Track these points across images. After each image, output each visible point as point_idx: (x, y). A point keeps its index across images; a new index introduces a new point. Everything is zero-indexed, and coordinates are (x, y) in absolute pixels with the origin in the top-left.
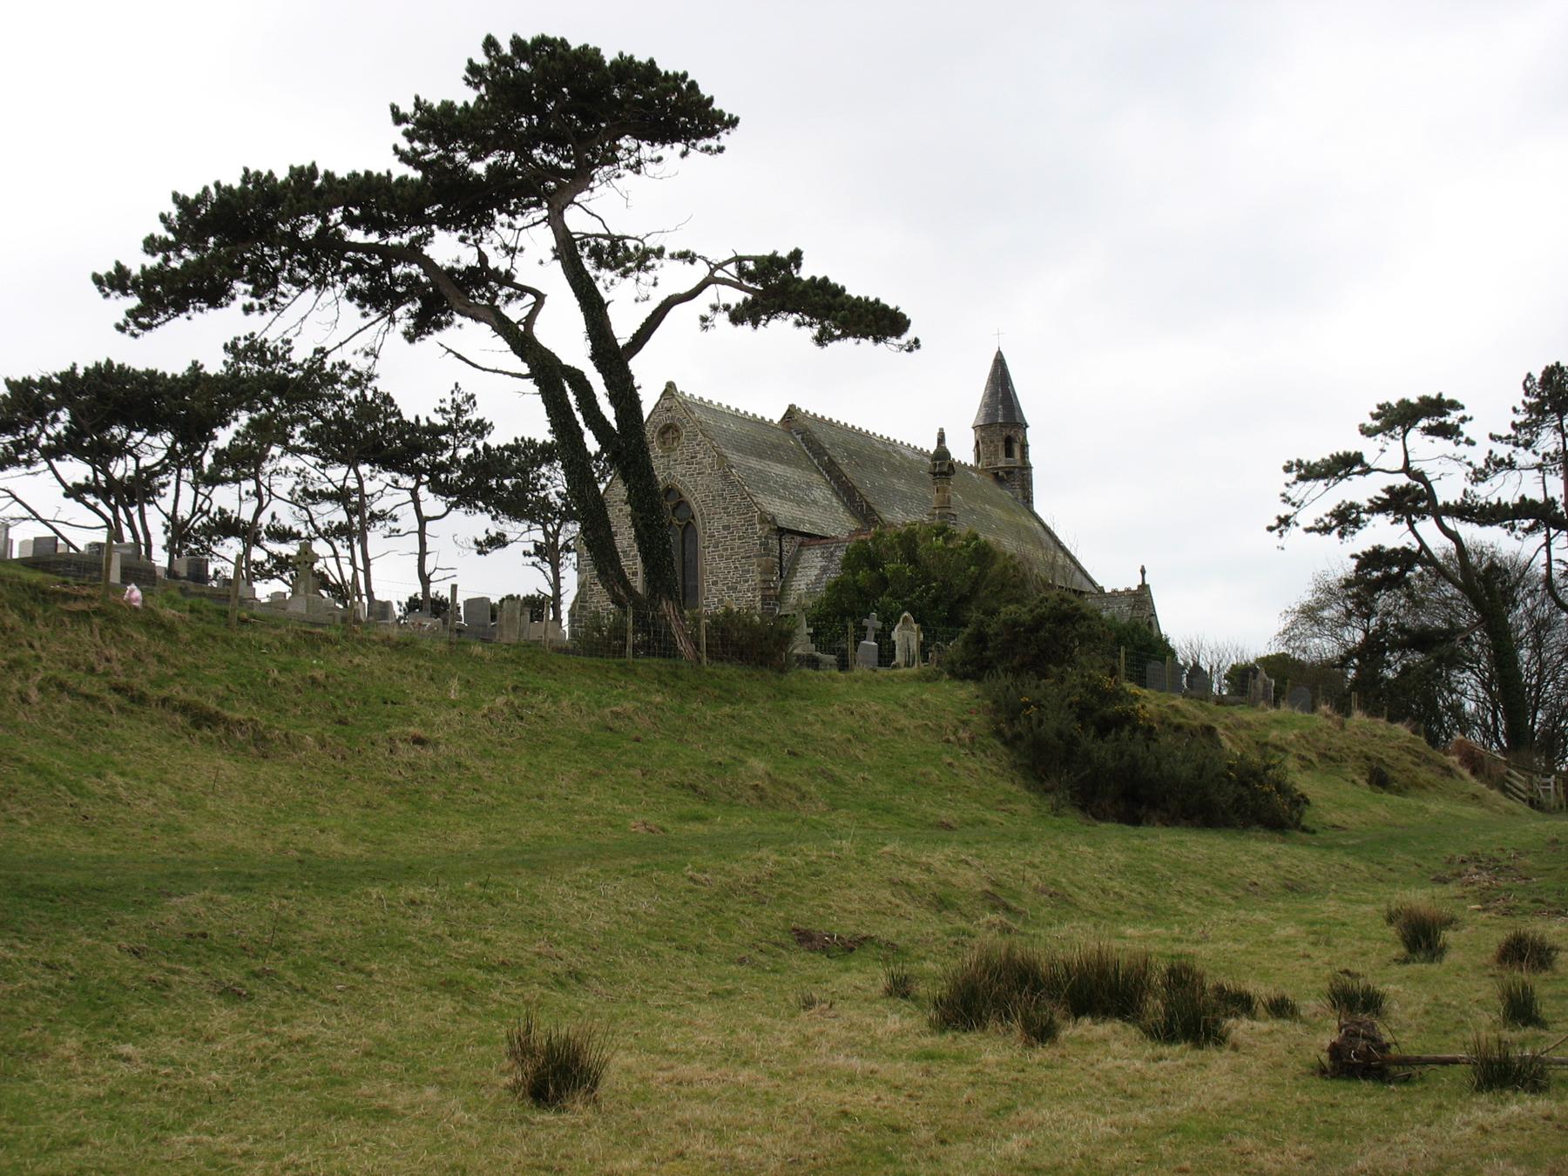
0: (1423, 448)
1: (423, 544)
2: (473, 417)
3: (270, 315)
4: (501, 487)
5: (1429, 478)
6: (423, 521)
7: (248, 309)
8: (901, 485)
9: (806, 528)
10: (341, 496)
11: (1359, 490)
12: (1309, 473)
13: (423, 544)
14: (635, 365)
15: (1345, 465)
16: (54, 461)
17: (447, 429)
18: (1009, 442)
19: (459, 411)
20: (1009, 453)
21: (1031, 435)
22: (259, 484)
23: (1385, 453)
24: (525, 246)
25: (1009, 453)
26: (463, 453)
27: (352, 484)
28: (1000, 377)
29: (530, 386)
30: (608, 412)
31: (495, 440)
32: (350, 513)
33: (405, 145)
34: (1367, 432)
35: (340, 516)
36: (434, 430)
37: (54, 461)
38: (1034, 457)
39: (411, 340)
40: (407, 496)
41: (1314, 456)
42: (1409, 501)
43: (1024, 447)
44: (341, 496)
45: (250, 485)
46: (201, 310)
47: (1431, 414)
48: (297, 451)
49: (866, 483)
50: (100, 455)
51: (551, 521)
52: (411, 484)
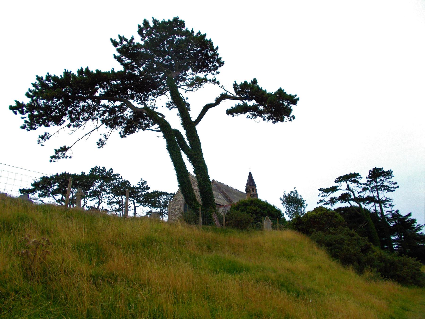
0: (352, 185)
1: (135, 212)
2: (145, 185)
3: (75, 128)
4: (151, 201)
5: (353, 191)
6: (135, 207)
7: (69, 126)
8: (236, 196)
9: (219, 204)
10: (118, 203)
11: (337, 194)
12: (327, 191)
13: (135, 212)
14: (198, 127)
15: (334, 189)
16: (54, 196)
17: (140, 188)
18: (253, 189)
19: (143, 185)
20: (253, 191)
21: (257, 188)
22: (99, 199)
23: (343, 185)
24: (161, 103)
25: (253, 191)
26: (143, 193)
27: (120, 199)
28: (250, 177)
29: (161, 134)
30: (184, 157)
31: (150, 191)
32: (120, 206)
33: (118, 54)
34: (336, 182)
35: (117, 206)
36: (137, 188)
37: (54, 196)
38: (258, 192)
39: (122, 137)
40: (132, 202)
41: (325, 188)
42: (344, 198)
43: (256, 190)
44: (118, 203)
45: (97, 200)
46: (54, 125)
47: (351, 177)
48: (108, 193)
49: (229, 195)
50: (64, 193)
51: (161, 207)
52: (133, 199)
